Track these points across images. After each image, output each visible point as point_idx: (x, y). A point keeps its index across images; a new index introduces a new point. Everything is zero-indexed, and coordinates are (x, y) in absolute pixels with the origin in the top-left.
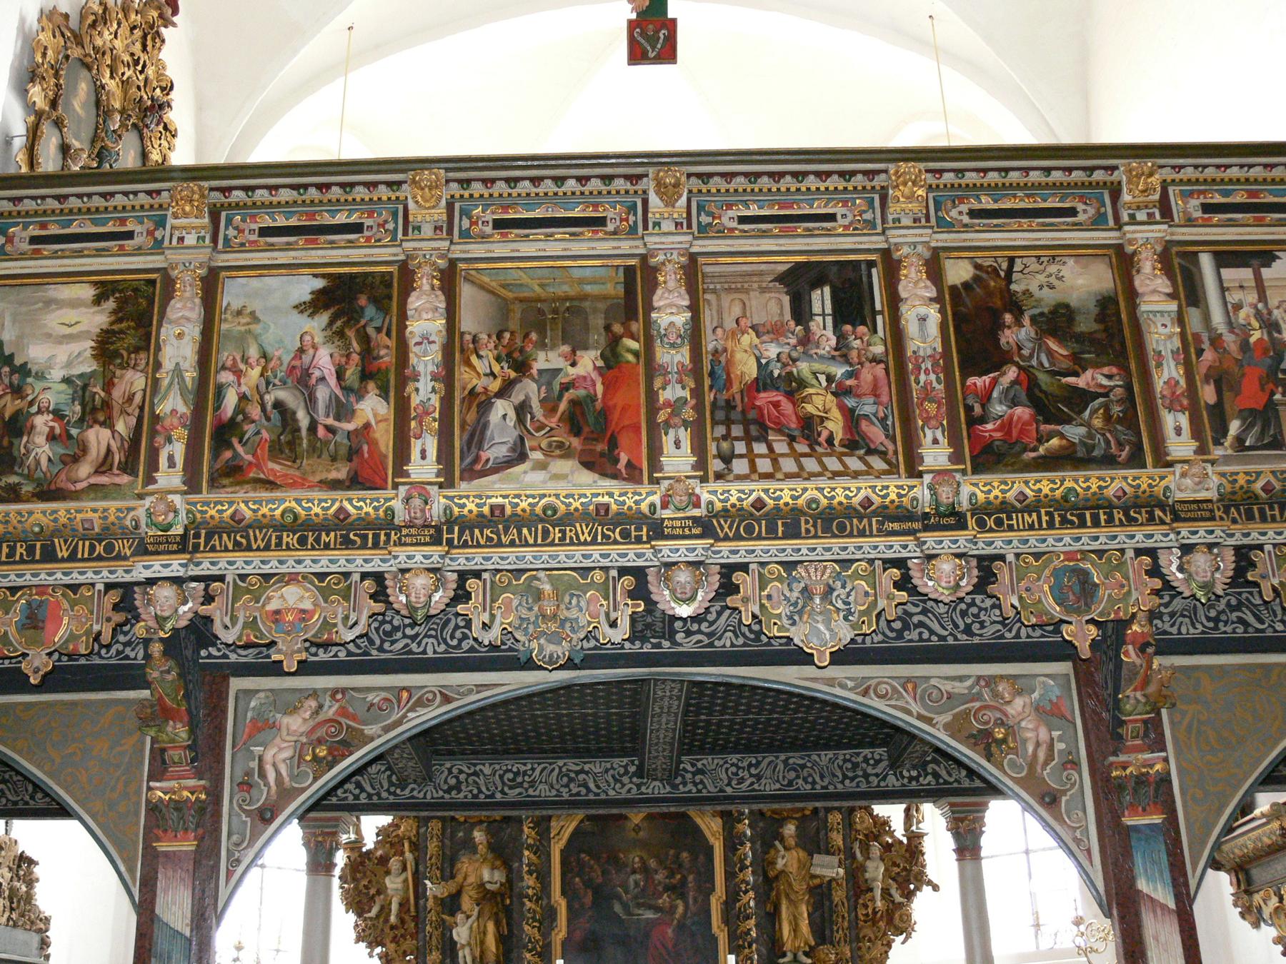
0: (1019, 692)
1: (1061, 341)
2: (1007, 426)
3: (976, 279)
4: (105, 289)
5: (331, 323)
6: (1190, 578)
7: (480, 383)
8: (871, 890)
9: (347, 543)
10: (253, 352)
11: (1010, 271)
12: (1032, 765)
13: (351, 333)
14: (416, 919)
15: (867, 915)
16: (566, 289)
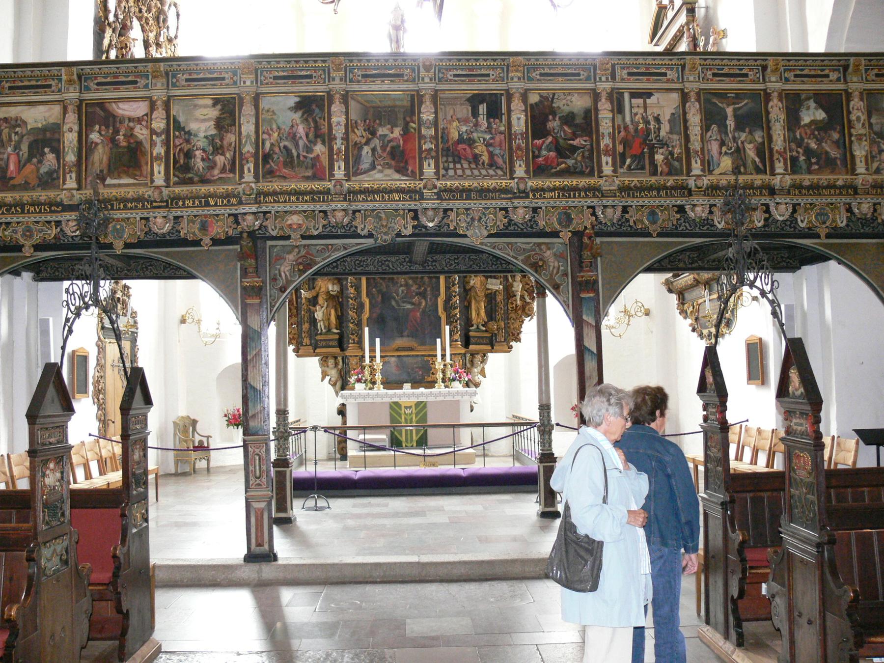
0: (549, 249)
1: (569, 126)
2: (547, 159)
3: (540, 101)
4: (216, 102)
5: (303, 115)
6: (605, 217)
7: (358, 140)
9: (313, 200)
10: (274, 127)
11: (553, 99)
12: (551, 275)
13: (310, 120)
14: (297, 308)
16: (389, 103)
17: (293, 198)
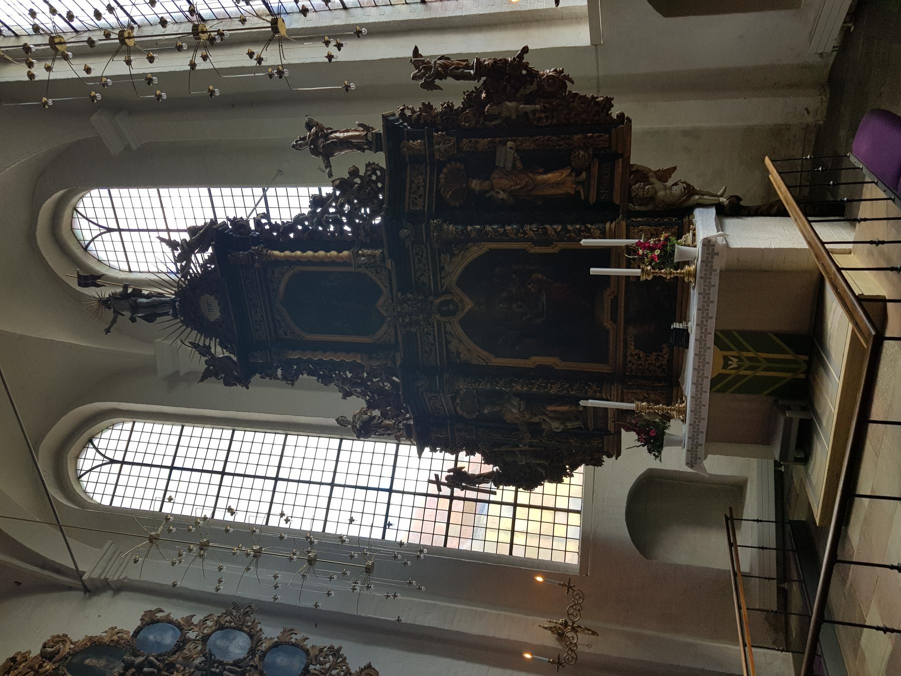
8: (526, 113)
15: (547, 118)
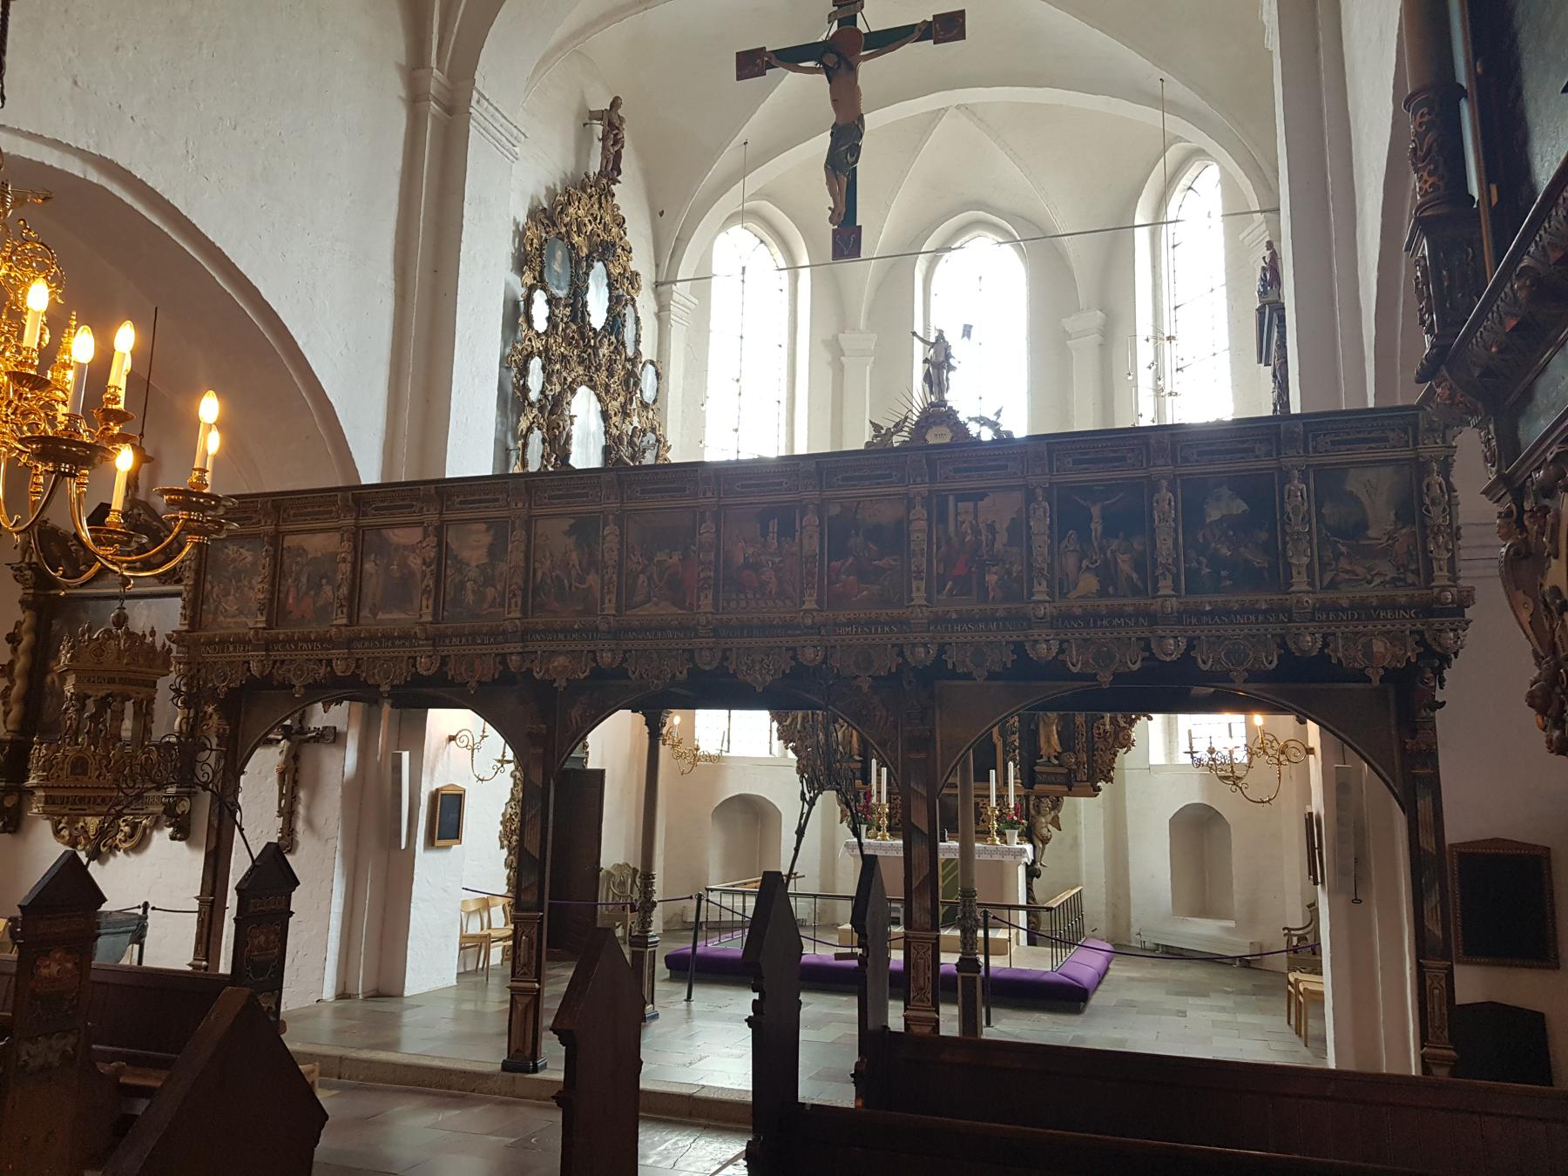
17: (561, 636)
